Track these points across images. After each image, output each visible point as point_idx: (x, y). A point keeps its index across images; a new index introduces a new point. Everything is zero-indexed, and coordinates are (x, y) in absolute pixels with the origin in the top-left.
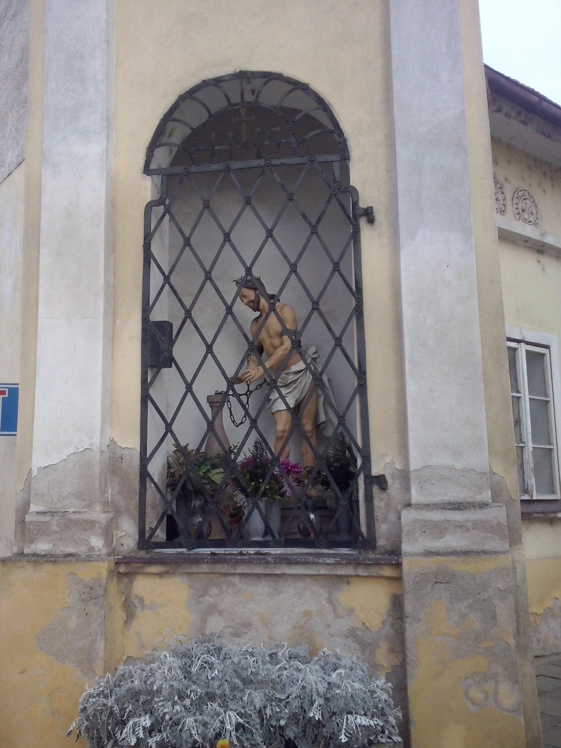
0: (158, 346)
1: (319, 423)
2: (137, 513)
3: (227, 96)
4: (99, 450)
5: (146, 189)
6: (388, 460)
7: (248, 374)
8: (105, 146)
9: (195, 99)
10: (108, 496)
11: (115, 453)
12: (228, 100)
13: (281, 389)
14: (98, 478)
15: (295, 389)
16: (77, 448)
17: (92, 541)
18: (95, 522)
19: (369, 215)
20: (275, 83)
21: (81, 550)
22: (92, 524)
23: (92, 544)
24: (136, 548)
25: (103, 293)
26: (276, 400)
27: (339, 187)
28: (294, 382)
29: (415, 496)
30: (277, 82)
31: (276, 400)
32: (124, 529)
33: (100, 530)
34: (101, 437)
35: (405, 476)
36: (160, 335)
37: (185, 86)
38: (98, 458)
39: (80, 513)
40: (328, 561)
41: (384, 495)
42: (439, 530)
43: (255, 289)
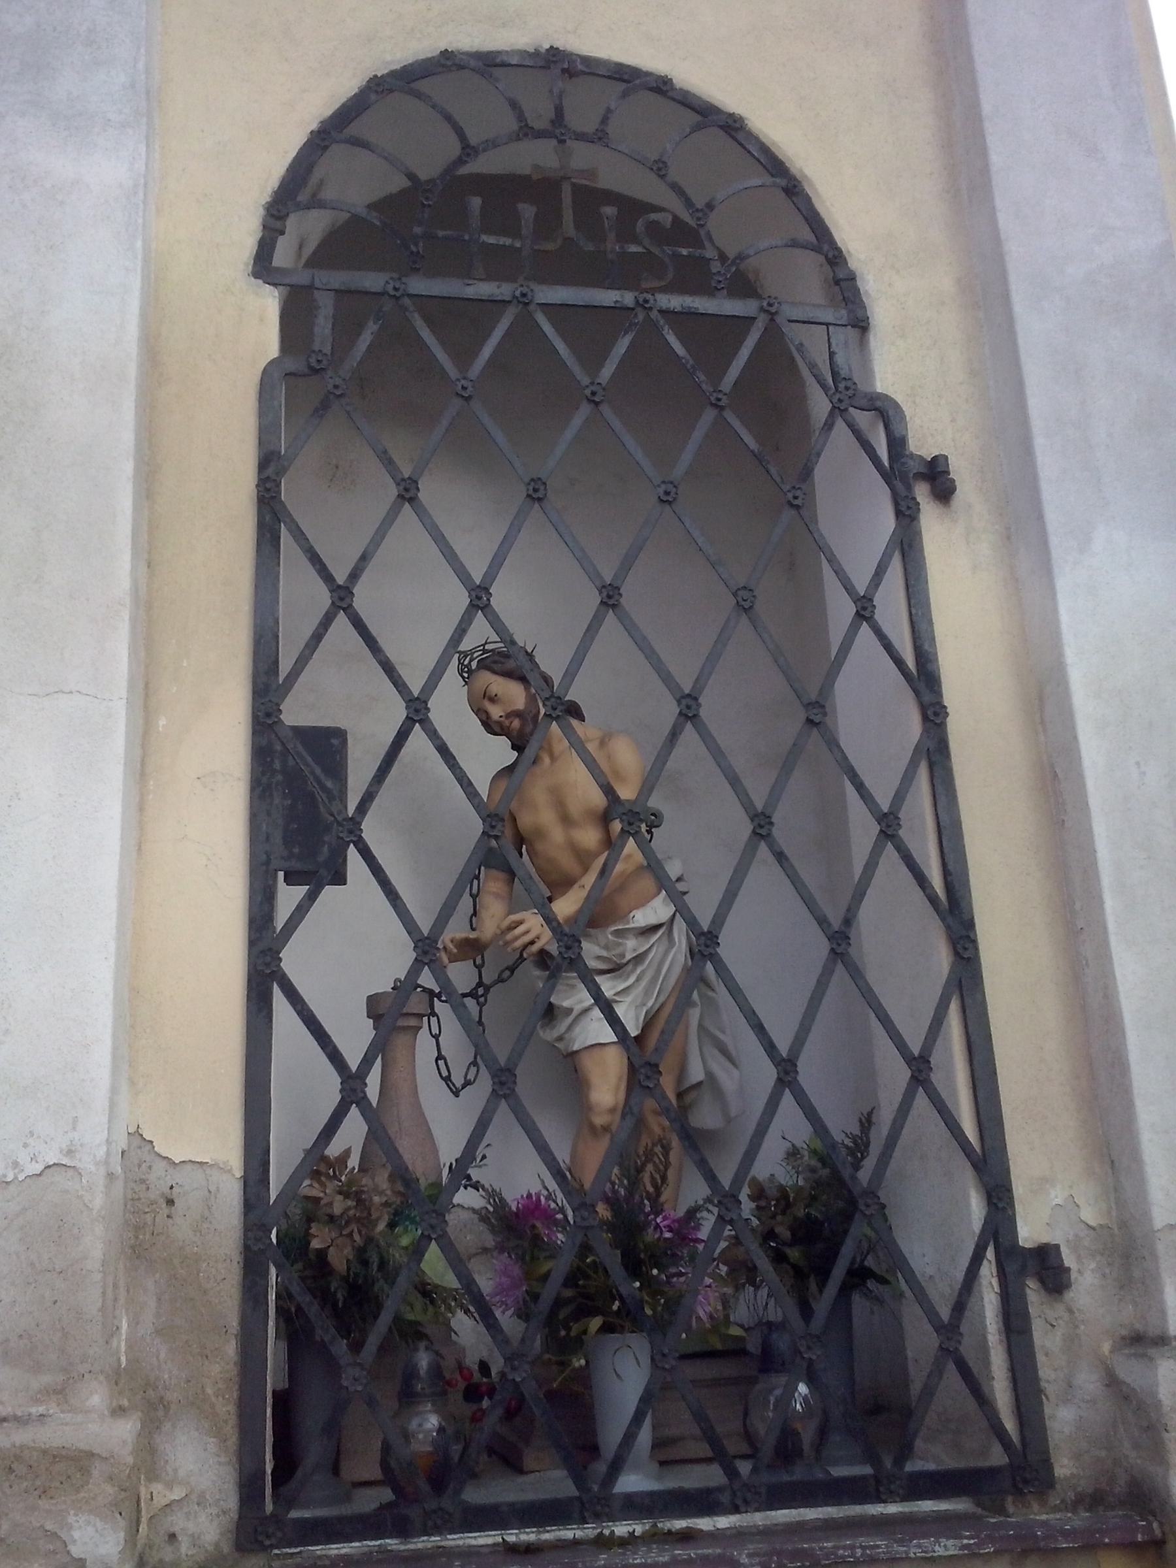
0: (302, 814)
1: (687, 1085)
2: (232, 1408)
3: (514, 105)
4: (102, 1171)
6: (1057, 1196)
7: (518, 931)
8: (140, 165)
9: (419, 95)
10: (119, 1346)
11: (143, 1181)
12: (521, 117)
13: (599, 979)
14: (98, 1277)
15: (638, 980)
16: (16, 1164)
17: (76, 1534)
18: (91, 1455)
19: (938, 477)
22: (69, 1468)
23: (76, 1551)
24: (226, 1548)
25: (126, 615)
26: (586, 1011)
27: (850, 393)
28: (639, 959)
30: (653, 97)
31: (586, 1011)
32: (182, 1473)
33: (110, 1490)
34: (109, 1122)
36: (318, 771)
37: (388, 58)
38: (98, 1201)
39: (21, 1421)
40: (940, 1551)
41: (1057, 1311)
43: (523, 679)
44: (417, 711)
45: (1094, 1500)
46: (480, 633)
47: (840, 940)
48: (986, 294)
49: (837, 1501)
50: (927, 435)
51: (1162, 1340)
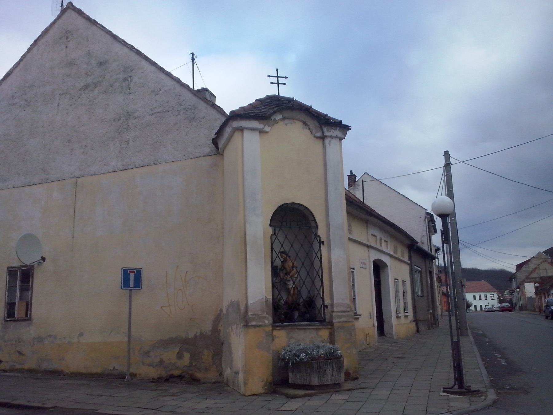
5: (270, 230)
19: (323, 242)
20: (94, 28)
21: (263, 324)
29: (335, 310)
35: (332, 305)
42: (340, 317)
44: (278, 255)
45: (329, 323)
46: (282, 250)
47: (313, 282)
48: (328, 225)
49: (307, 389)
50: (323, 238)
51: (42, 257)
